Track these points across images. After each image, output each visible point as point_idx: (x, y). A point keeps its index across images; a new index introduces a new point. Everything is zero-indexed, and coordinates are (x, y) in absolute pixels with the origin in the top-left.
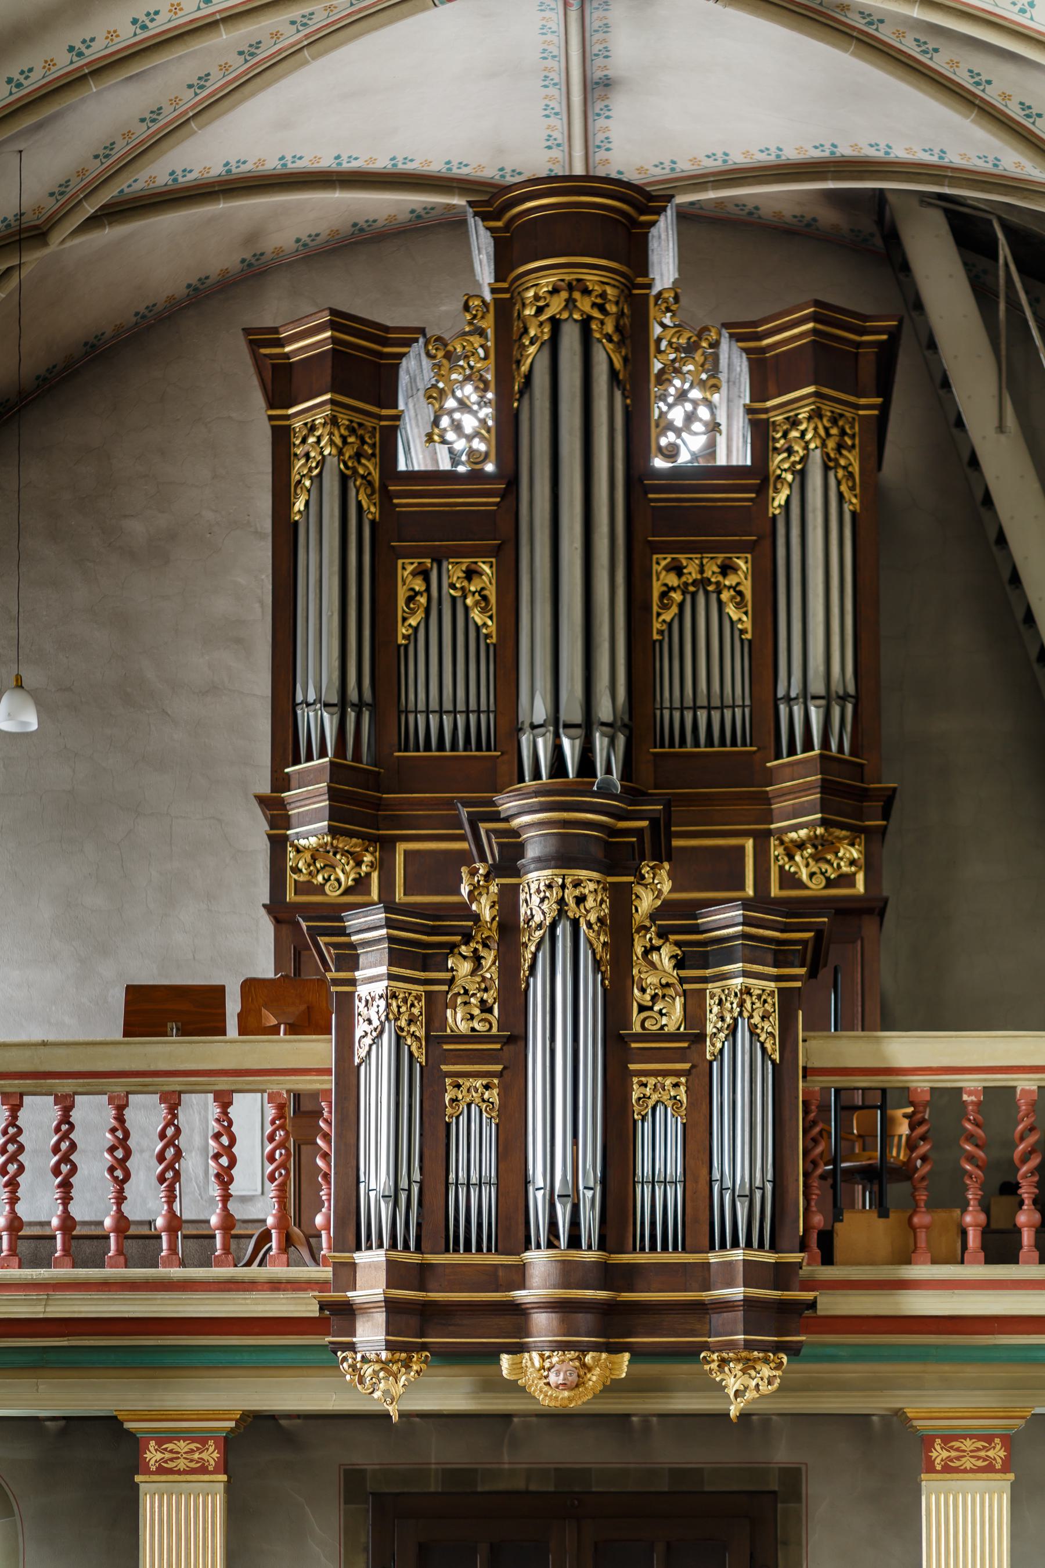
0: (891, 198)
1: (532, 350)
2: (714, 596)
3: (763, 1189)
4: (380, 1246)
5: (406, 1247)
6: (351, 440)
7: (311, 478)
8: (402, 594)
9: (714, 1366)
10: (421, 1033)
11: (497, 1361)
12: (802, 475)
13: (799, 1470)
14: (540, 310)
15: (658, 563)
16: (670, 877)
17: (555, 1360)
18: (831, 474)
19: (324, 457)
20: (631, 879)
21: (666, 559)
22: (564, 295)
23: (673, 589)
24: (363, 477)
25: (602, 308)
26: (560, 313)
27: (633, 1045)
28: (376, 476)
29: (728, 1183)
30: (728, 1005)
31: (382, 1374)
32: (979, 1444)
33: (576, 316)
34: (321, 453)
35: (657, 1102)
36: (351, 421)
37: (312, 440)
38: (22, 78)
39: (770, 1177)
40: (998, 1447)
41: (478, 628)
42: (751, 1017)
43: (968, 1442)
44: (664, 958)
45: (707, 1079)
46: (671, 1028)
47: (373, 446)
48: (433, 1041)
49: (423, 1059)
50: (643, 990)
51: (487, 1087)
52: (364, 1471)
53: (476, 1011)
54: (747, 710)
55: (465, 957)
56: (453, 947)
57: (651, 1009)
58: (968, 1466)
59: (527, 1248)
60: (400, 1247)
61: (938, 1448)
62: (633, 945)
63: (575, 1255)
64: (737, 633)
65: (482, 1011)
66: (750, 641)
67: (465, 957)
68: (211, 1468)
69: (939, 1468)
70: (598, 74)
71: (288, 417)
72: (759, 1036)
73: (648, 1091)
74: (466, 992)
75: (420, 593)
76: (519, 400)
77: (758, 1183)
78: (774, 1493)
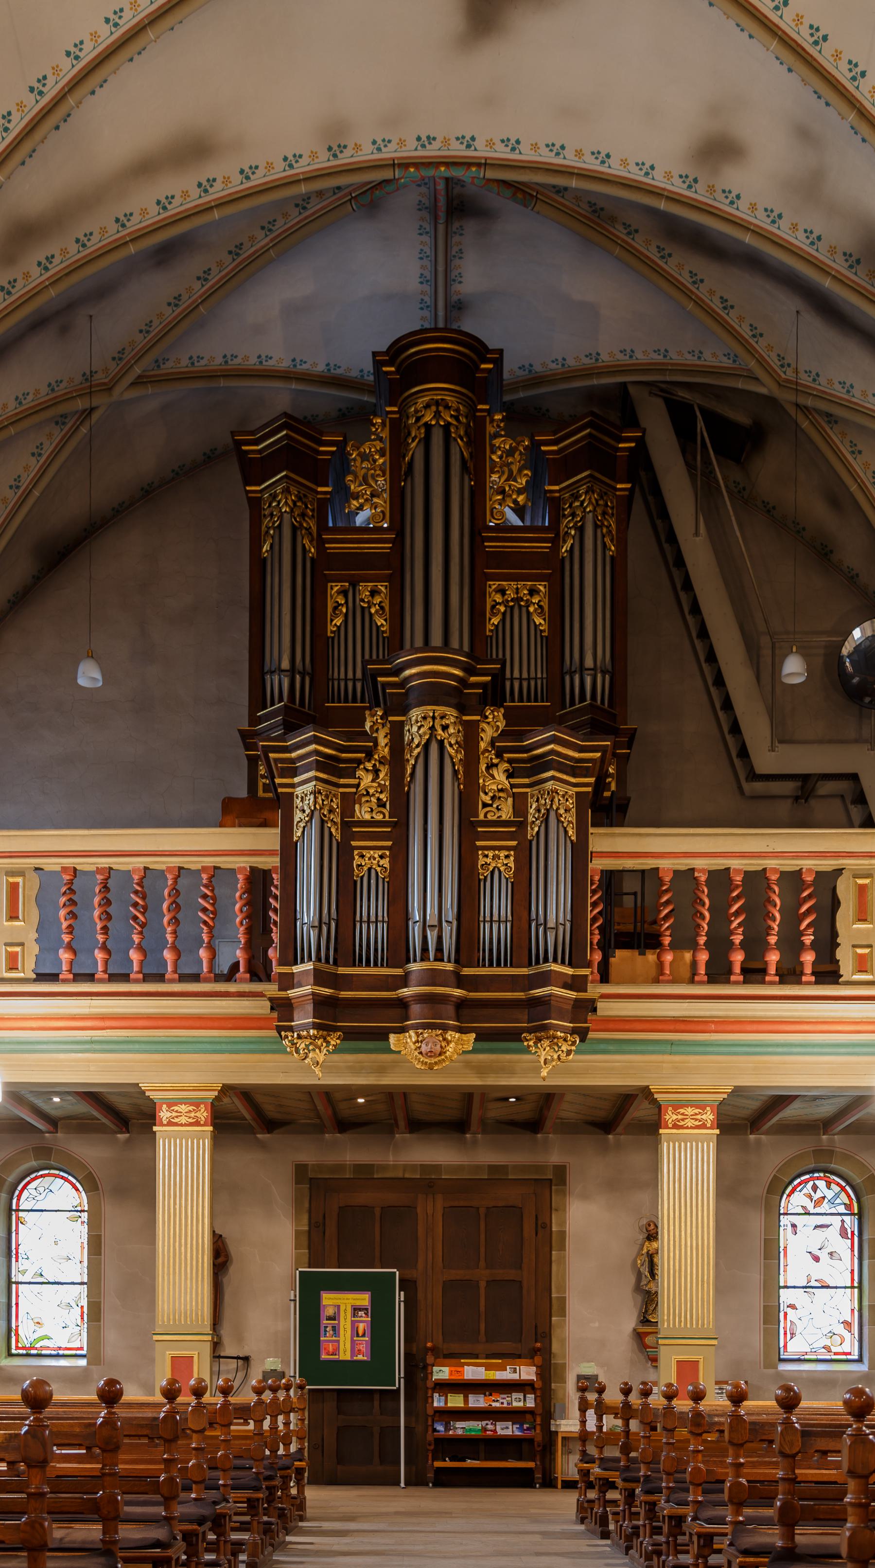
0: (632, 390)
1: (414, 445)
2: (524, 610)
3: (564, 925)
4: (310, 959)
5: (327, 961)
6: (299, 504)
7: (274, 529)
8: (330, 605)
9: (531, 1043)
10: (338, 820)
11: (387, 1039)
12: (581, 530)
13: (565, 1166)
14: (418, 419)
15: (490, 587)
16: (504, 717)
17: (426, 1035)
18: (599, 531)
19: (282, 513)
20: (478, 718)
21: (494, 585)
22: (434, 408)
23: (500, 604)
24: (306, 529)
25: (456, 418)
26: (431, 420)
27: (479, 829)
28: (314, 529)
29: (542, 920)
30: (543, 802)
31: (311, 1047)
32: (697, 1111)
33: (442, 423)
34: (280, 511)
35: (494, 868)
36: (299, 492)
37: (274, 504)
38: (85, 239)
39: (569, 917)
40: (709, 1113)
41: (378, 627)
42: (558, 809)
43: (689, 1110)
44: (500, 776)
45: (528, 852)
46: (504, 818)
47: (313, 510)
48: (346, 826)
49: (339, 837)
50: (486, 794)
51: (381, 857)
52: (306, 1165)
53: (375, 807)
54: (545, 681)
55: (367, 770)
56: (359, 762)
57: (491, 805)
58: (690, 1125)
59: (408, 961)
60: (323, 960)
61: (670, 1113)
62: (479, 763)
63: (439, 966)
64: (539, 632)
65: (379, 806)
66: (547, 637)
67: (367, 770)
68: (202, 1123)
69: (670, 1126)
70: (455, 298)
71: (293, 786)
72: (563, 822)
73: (488, 861)
74: (368, 793)
75: (342, 605)
76: (405, 481)
77: (561, 920)
78: (551, 1180)
